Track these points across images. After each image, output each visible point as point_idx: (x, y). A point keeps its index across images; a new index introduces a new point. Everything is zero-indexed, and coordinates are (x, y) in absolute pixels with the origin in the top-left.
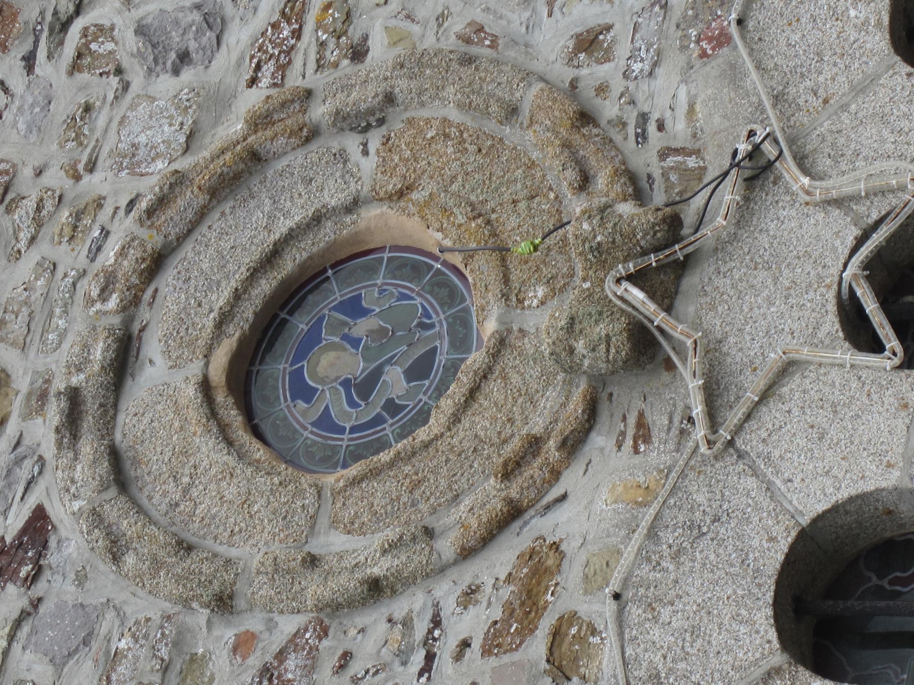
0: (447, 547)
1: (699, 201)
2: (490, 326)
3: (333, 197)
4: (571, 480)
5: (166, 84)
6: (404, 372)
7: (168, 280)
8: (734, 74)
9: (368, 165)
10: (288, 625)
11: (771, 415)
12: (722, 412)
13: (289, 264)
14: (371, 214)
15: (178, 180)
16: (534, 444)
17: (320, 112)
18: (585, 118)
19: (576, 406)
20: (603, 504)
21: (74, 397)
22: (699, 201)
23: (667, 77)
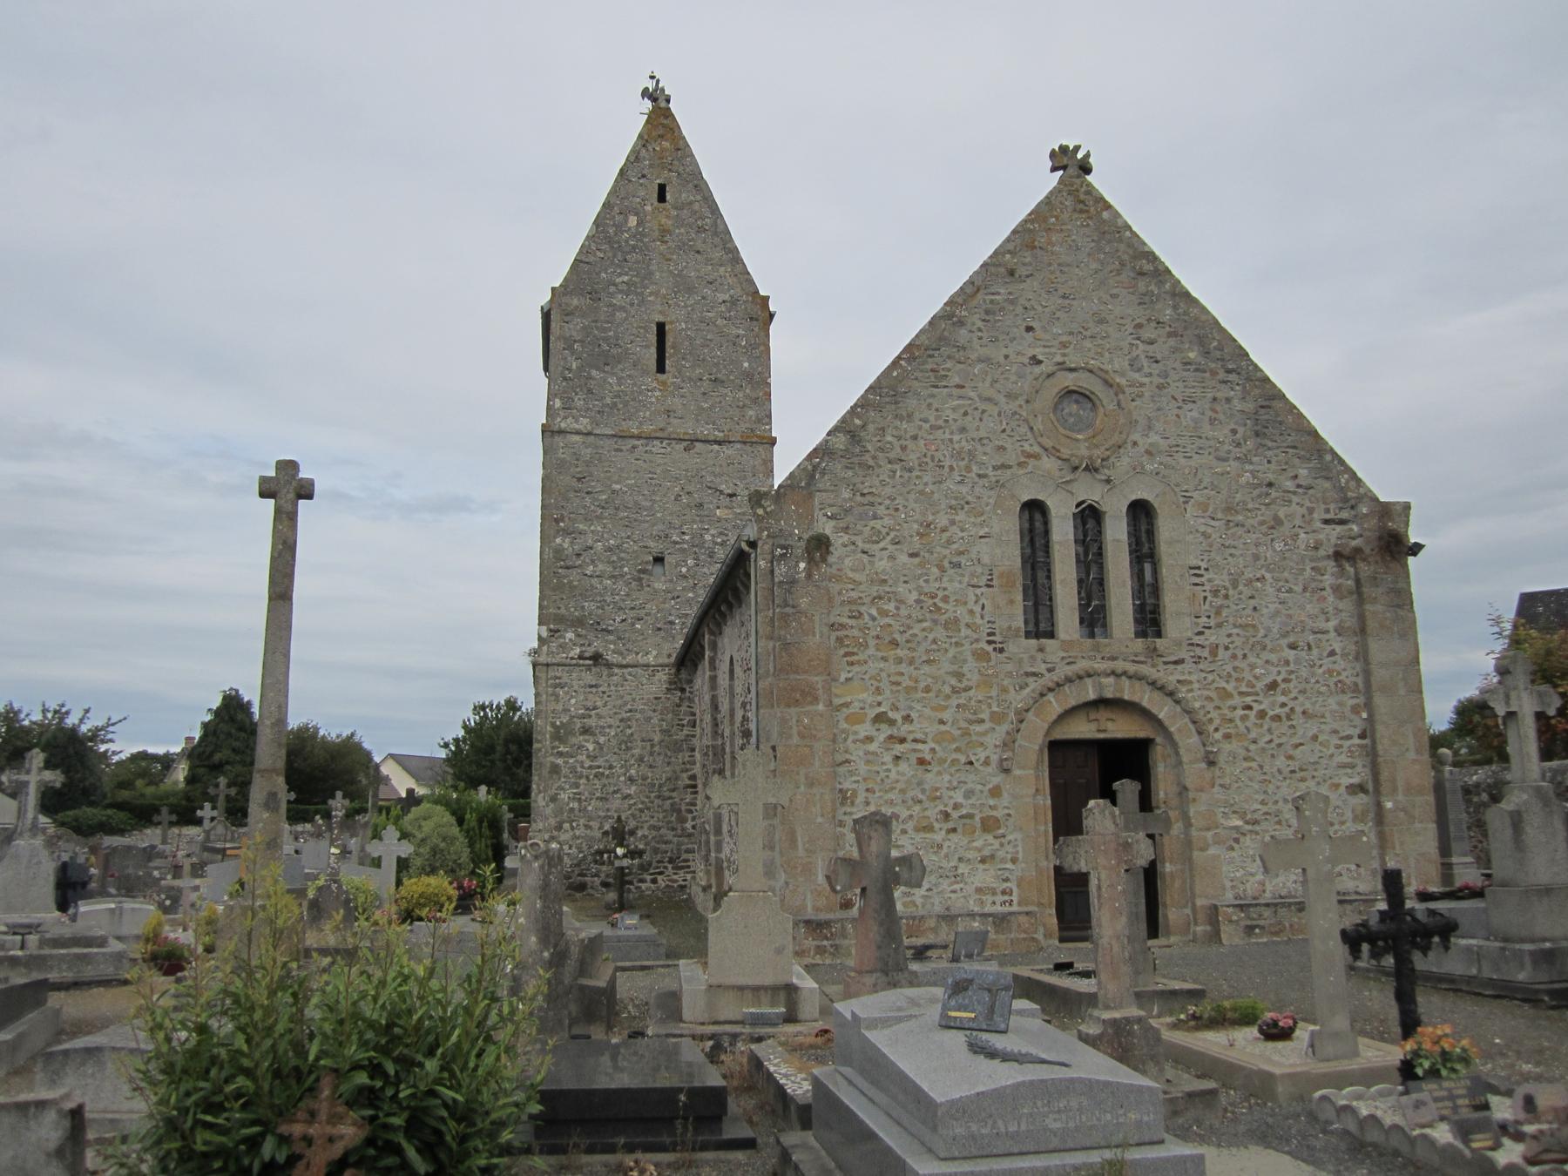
0: (1040, 439)
1: (1270, 444)
2: (1080, 437)
3: (1105, 402)
4: (1053, 459)
5: (1127, 363)
6: (1271, 1076)
7: (1088, 374)
8: (1128, 473)
9: (1111, 407)
10: (1024, 414)
11: (1064, 493)
12: (540, 750)
13: (1092, 397)
14: (1101, 410)
15: (1107, 372)
16: (1058, 451)
17: (1121, 396)
18: (1120, 447)
19: (1065, 457)
20: (1048, 466)
21: (1064, 363)
22: (1270, 444)
23: (1128, 460)
